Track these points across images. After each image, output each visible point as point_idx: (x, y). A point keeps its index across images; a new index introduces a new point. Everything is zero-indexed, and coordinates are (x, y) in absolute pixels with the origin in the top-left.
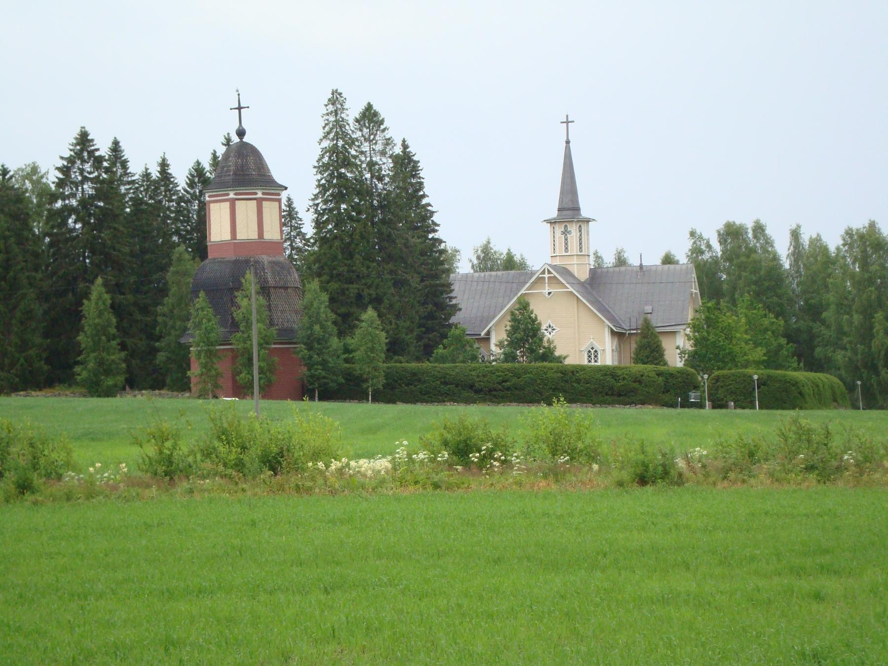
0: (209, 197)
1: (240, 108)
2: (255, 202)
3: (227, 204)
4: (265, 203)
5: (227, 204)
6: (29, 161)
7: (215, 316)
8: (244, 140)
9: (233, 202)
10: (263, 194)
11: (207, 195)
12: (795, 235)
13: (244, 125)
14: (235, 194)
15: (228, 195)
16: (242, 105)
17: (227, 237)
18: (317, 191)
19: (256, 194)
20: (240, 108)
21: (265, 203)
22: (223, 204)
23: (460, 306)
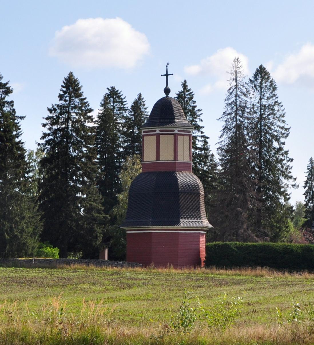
0: (144, 132)
1: (167, 75)
2: (173, 136)
3: (155, 137)
4: (179, 137)
5: (155, 137)
6: (208, 142)
7: (300, 246)
8: (169, 96)
9: (158, 136)
10: (179, 131)
11: (142, 131)
12: (83, 92)
13: (170, 86)
14: (160, 131)
15: (155, 131)
16: (165, 73)
17: (153, 158)
18: (277, 142)
19: (174, 131)
20: (167, 75)
21: (179, 137)
22: (154, 136)
23: (22, 141)
